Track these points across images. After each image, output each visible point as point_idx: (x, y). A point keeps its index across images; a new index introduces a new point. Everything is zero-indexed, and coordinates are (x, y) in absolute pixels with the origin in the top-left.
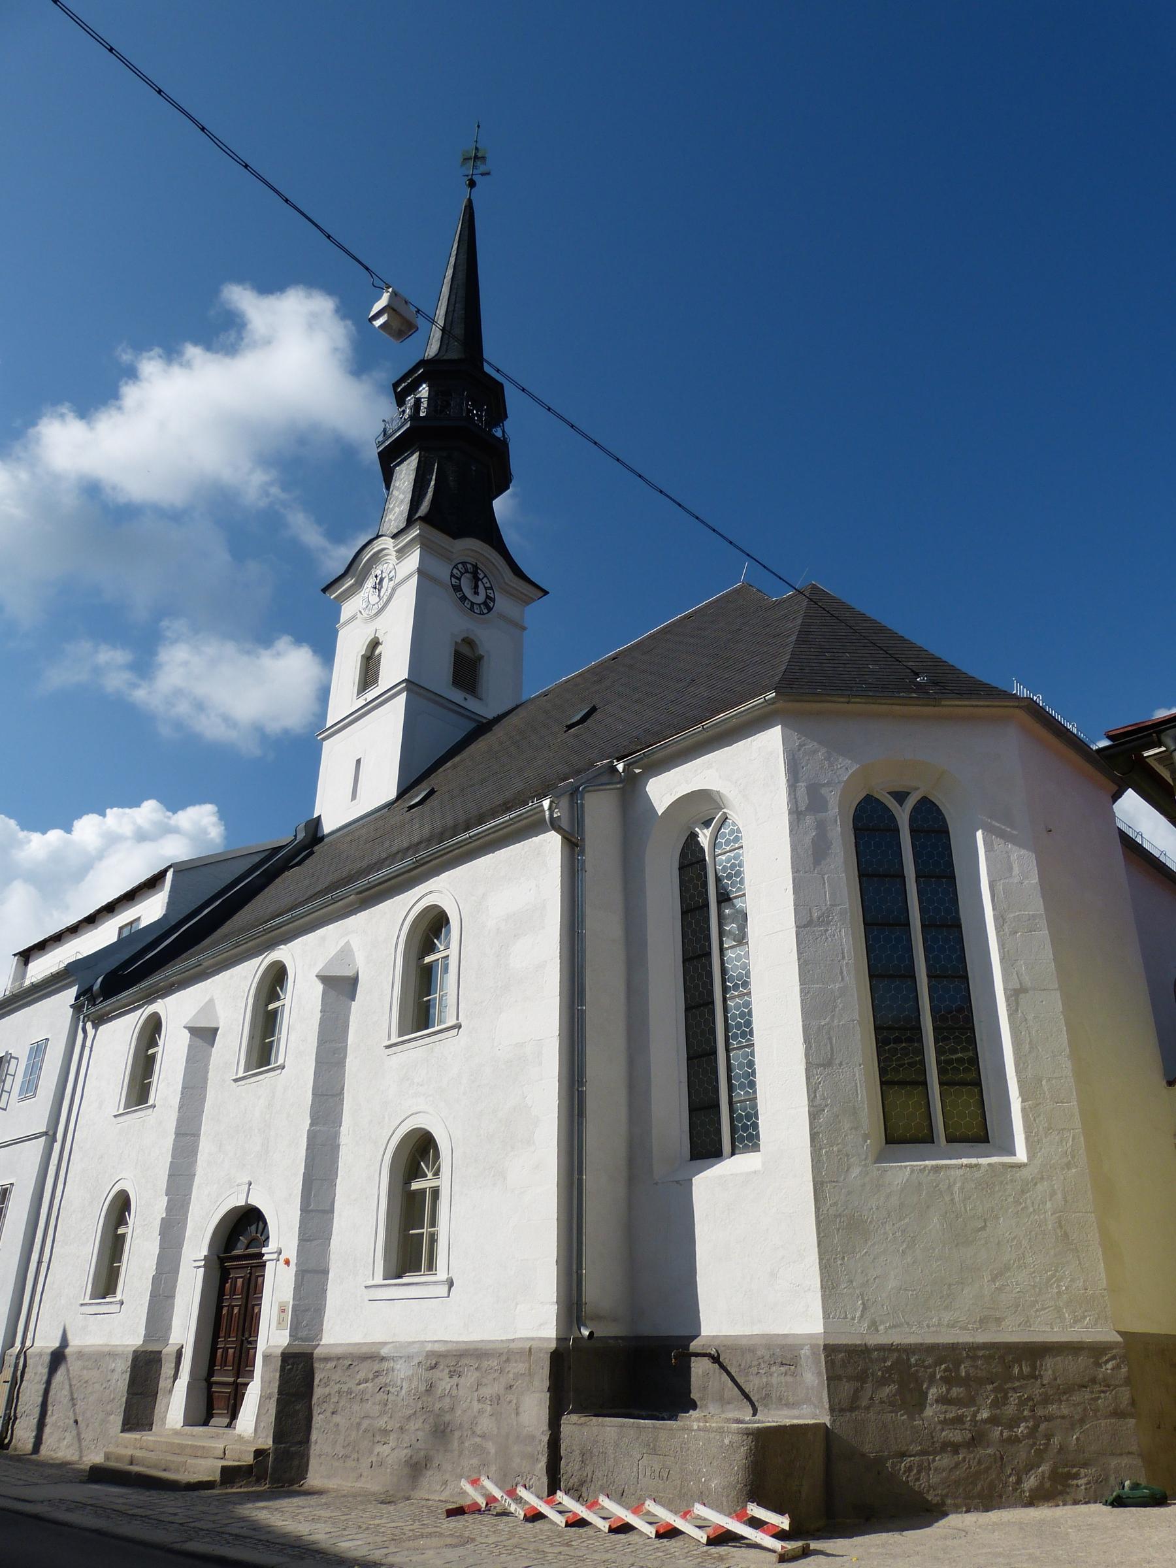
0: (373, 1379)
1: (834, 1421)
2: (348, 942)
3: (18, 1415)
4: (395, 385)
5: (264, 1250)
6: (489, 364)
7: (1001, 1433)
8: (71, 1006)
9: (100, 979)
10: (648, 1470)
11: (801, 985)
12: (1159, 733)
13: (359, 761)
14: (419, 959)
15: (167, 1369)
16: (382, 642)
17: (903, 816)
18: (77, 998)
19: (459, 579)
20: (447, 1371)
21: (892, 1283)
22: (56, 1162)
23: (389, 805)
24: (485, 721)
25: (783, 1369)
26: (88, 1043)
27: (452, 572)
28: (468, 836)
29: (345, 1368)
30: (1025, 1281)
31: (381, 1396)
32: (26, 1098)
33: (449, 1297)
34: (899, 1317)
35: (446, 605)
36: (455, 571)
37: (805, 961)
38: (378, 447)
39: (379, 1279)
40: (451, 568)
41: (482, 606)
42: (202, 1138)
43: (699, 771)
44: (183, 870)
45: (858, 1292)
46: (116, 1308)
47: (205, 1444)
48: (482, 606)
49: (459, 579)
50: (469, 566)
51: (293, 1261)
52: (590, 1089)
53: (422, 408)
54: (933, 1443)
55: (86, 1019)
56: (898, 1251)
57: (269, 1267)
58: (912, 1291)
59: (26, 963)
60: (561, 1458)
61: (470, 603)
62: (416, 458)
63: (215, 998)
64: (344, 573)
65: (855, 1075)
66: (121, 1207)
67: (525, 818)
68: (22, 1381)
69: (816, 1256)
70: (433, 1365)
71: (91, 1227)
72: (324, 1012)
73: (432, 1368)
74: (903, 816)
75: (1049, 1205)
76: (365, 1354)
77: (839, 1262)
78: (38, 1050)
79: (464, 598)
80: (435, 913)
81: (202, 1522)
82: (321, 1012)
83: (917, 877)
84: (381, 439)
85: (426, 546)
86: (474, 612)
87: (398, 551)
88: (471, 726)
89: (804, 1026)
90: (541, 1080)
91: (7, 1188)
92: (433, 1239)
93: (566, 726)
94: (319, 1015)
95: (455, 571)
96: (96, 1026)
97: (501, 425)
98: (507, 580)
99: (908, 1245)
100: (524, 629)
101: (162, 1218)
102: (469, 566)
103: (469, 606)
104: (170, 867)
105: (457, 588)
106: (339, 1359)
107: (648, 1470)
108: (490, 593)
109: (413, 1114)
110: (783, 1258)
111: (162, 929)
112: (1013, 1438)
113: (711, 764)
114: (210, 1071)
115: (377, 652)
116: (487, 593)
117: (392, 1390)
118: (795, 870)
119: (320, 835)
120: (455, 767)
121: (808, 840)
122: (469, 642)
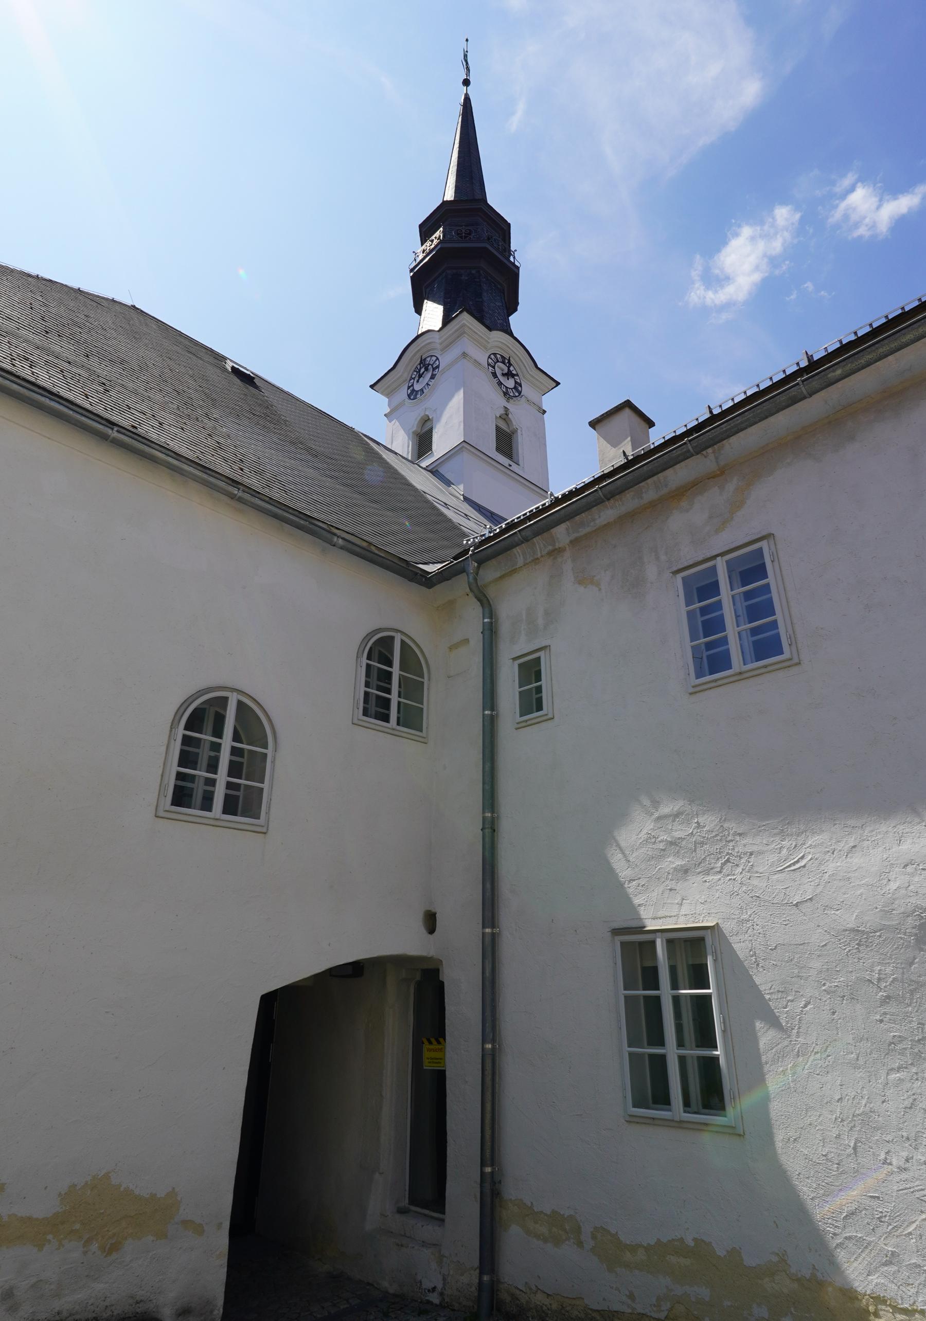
6: (477, 363)
16: (433, 418)
19: (494, 367)
36: (490, 361)
40: (487, 359)
41: (513, 390)
48: (513, 390)
50: (498, 356)
95: (490, 361)
100: (544, 412)
112: (89, 1183)
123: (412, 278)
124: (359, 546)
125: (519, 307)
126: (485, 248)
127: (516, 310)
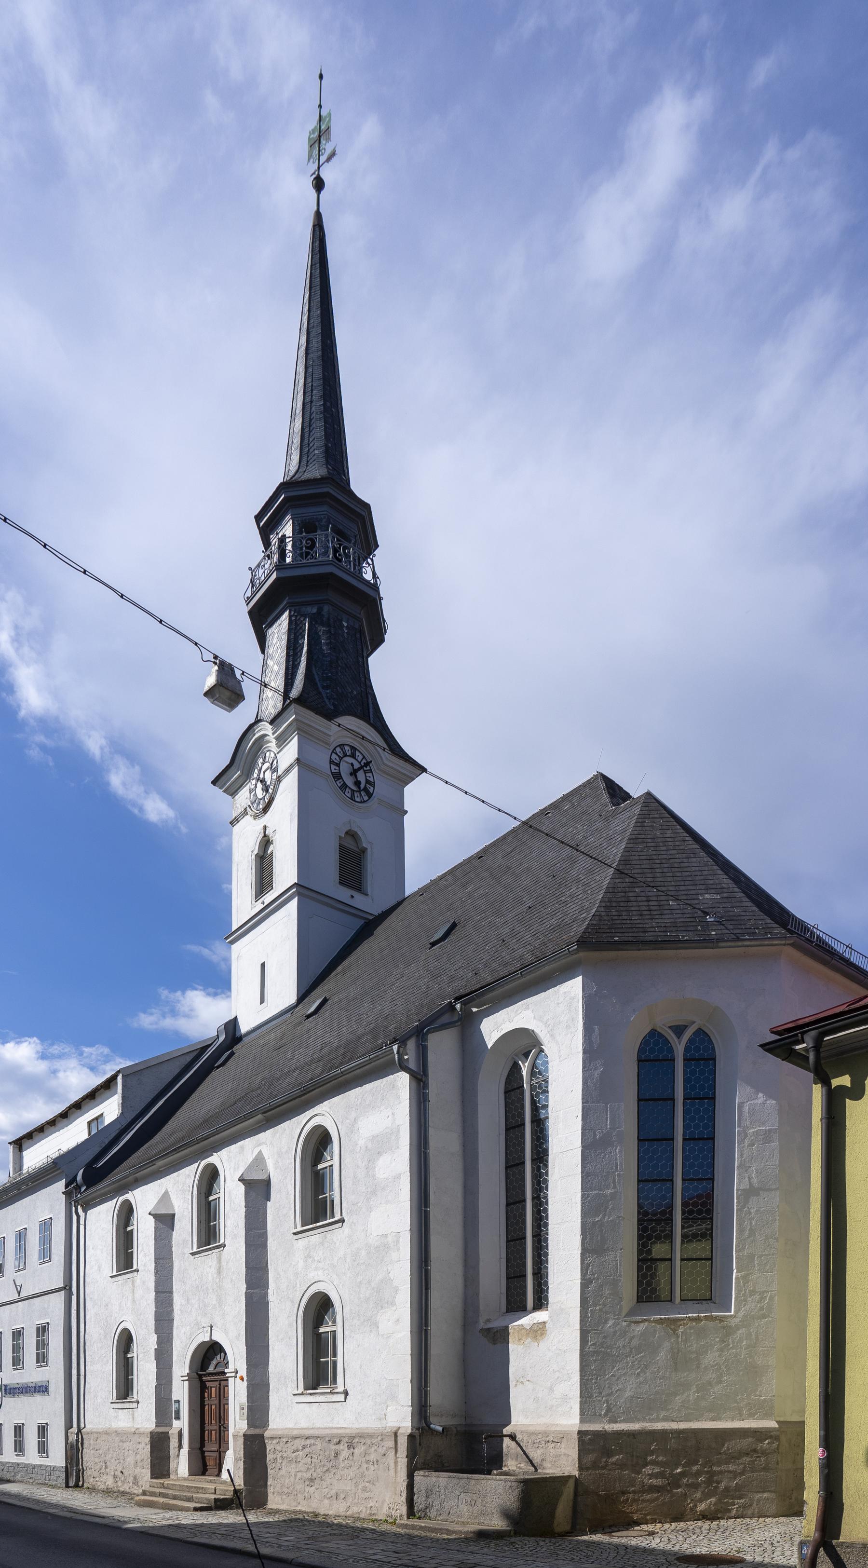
0: (302, 1450)
1: (581, 1474)
2: (260, 1151)
3: (85, 1469)
4: (258, 518)
5: (226, 1371)
7: (688, 1481)
8: (63, 1193)
9: (81, 1172)
10: (464, 1501)
11: (582, 1191)
12: (803, 1033)
13: (263, 965)
14: (314, 1166)
15: (174, 1443)
17: (679, 1048)
18: (66, 1187)
19: (338, 765)
20: (346, 1445)
21: (628, 1394)
22: (75, 1308)
23: (291, 1009)
24: (371, 918)
25: (553, 1445)
26: (82, 1222)
27: (331, 758)
28: (340, 1071)
29: (284, 1443)
30: (719, 1391)
31: (308, 1460)
32: (44, 1262)
33: (345, 1401)
34: (631, 1415)
35: (327, 792)
36: (334, 756)
37: (587, 1173)
38: (247, 605)
39: (301, 1389)
42: (175, 1295)
43: (519, 1012)
44: (129, 1074)
45: (604, 1399)
46: (135, 1405)
47: (203, 1486)
49: (338, 765)
50: (347, 748)
51: (245, 1378)
52: (434, 1268)
53: (287, 551)
54: (644, 1486)
55: (76, 1204)
56: (635, 1374)
57: (231, 1381)
58: (641, 1398)
59: (21, 1150)
60: (415, 1494)
61: (350, 791)
62: (286, 618)
63: (169, 1191)
64: (230, 763)
65: (616, 1257)
66: (126, 1341)
67: (381, 1058)
68: (83, 1449)
69: (578, 1377)
70: (337, 1442)
71: (108, 1353)
72: (248, 1207)
73: (337, 1444)
74: (679, 1048)
75: (744, 1343)
76: (296, 1435)
77: (593, 1381)
78: (46, 1226)
79: (344, 787)
80: (321, 1130)
81: (203, 1528)
82: (245, 1207)
83: (685, 1099)
84: (249, 594)
85: (301, 728)
86: (355, 801)
87: (277, 739)
88: (359, 923)
89: (582, 1222)
90: (399, 1261)
91: (45, 1326)
92: (335, 1363)
93: (430, 944)
94: (244, 1210)
95: (334, 756)
96: (85, 1211)
97: (369, 561)
98: (386, 762)
99: (641, 1370)
101: (155, 1349)
102: (347, 748)
103: (349, 795)
104: (119, 1072)
105: (337, 776)
106: (280, 1438)
107: (464, 1501)
108: (370, 777)
109: (315, 1282)
110: (558, 1378)
111: (121, 1127)
113: (528, 1005)
114: (173, 1246)
115: (269, 851)
116: (366, 776)
117: (314, 1456)
118: (585, 1100)
119: (238, 1035)
120: (344, 972)
121: (597, 1074)
122: (352, 834)
123: (250, 613)
124: (352, 503)
125: (386, 637)
126: (331, 574)
127: (382, 641)
